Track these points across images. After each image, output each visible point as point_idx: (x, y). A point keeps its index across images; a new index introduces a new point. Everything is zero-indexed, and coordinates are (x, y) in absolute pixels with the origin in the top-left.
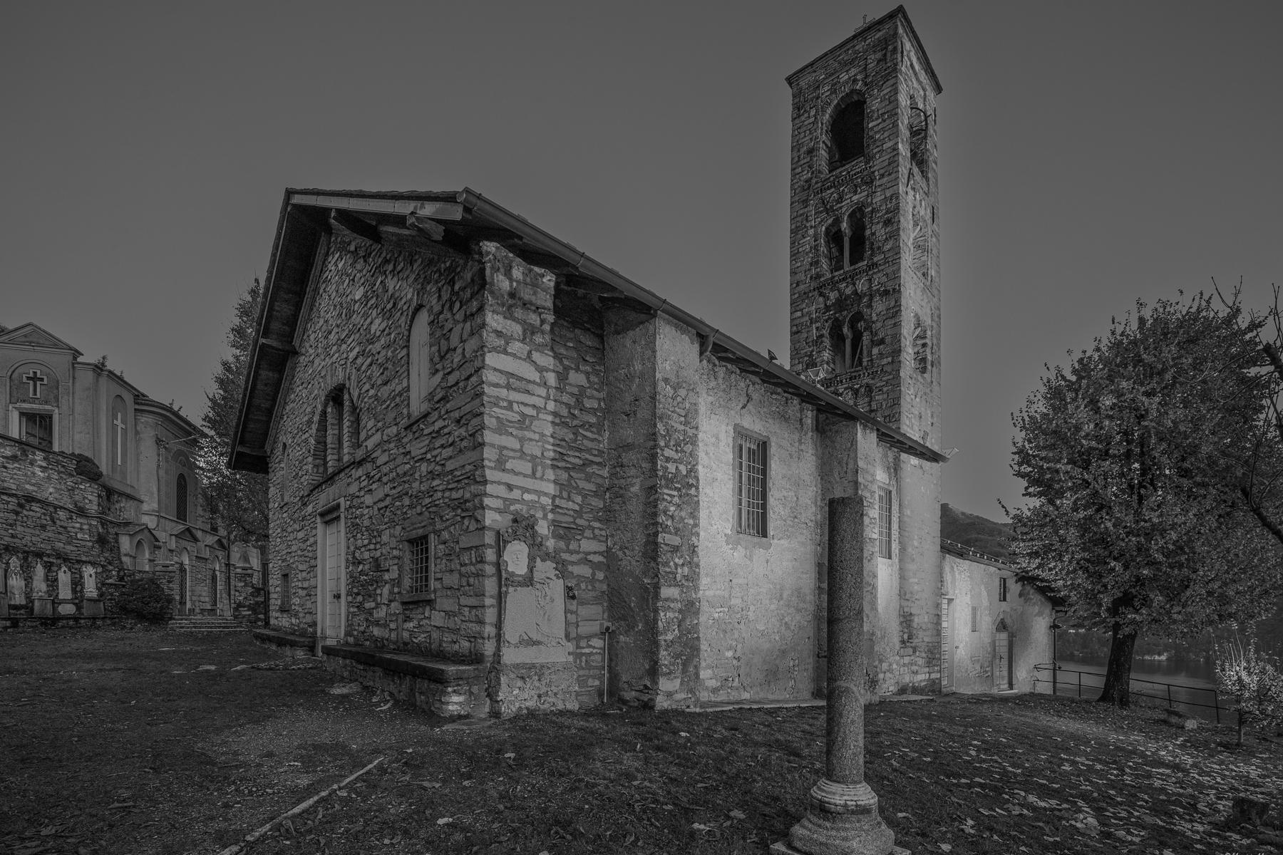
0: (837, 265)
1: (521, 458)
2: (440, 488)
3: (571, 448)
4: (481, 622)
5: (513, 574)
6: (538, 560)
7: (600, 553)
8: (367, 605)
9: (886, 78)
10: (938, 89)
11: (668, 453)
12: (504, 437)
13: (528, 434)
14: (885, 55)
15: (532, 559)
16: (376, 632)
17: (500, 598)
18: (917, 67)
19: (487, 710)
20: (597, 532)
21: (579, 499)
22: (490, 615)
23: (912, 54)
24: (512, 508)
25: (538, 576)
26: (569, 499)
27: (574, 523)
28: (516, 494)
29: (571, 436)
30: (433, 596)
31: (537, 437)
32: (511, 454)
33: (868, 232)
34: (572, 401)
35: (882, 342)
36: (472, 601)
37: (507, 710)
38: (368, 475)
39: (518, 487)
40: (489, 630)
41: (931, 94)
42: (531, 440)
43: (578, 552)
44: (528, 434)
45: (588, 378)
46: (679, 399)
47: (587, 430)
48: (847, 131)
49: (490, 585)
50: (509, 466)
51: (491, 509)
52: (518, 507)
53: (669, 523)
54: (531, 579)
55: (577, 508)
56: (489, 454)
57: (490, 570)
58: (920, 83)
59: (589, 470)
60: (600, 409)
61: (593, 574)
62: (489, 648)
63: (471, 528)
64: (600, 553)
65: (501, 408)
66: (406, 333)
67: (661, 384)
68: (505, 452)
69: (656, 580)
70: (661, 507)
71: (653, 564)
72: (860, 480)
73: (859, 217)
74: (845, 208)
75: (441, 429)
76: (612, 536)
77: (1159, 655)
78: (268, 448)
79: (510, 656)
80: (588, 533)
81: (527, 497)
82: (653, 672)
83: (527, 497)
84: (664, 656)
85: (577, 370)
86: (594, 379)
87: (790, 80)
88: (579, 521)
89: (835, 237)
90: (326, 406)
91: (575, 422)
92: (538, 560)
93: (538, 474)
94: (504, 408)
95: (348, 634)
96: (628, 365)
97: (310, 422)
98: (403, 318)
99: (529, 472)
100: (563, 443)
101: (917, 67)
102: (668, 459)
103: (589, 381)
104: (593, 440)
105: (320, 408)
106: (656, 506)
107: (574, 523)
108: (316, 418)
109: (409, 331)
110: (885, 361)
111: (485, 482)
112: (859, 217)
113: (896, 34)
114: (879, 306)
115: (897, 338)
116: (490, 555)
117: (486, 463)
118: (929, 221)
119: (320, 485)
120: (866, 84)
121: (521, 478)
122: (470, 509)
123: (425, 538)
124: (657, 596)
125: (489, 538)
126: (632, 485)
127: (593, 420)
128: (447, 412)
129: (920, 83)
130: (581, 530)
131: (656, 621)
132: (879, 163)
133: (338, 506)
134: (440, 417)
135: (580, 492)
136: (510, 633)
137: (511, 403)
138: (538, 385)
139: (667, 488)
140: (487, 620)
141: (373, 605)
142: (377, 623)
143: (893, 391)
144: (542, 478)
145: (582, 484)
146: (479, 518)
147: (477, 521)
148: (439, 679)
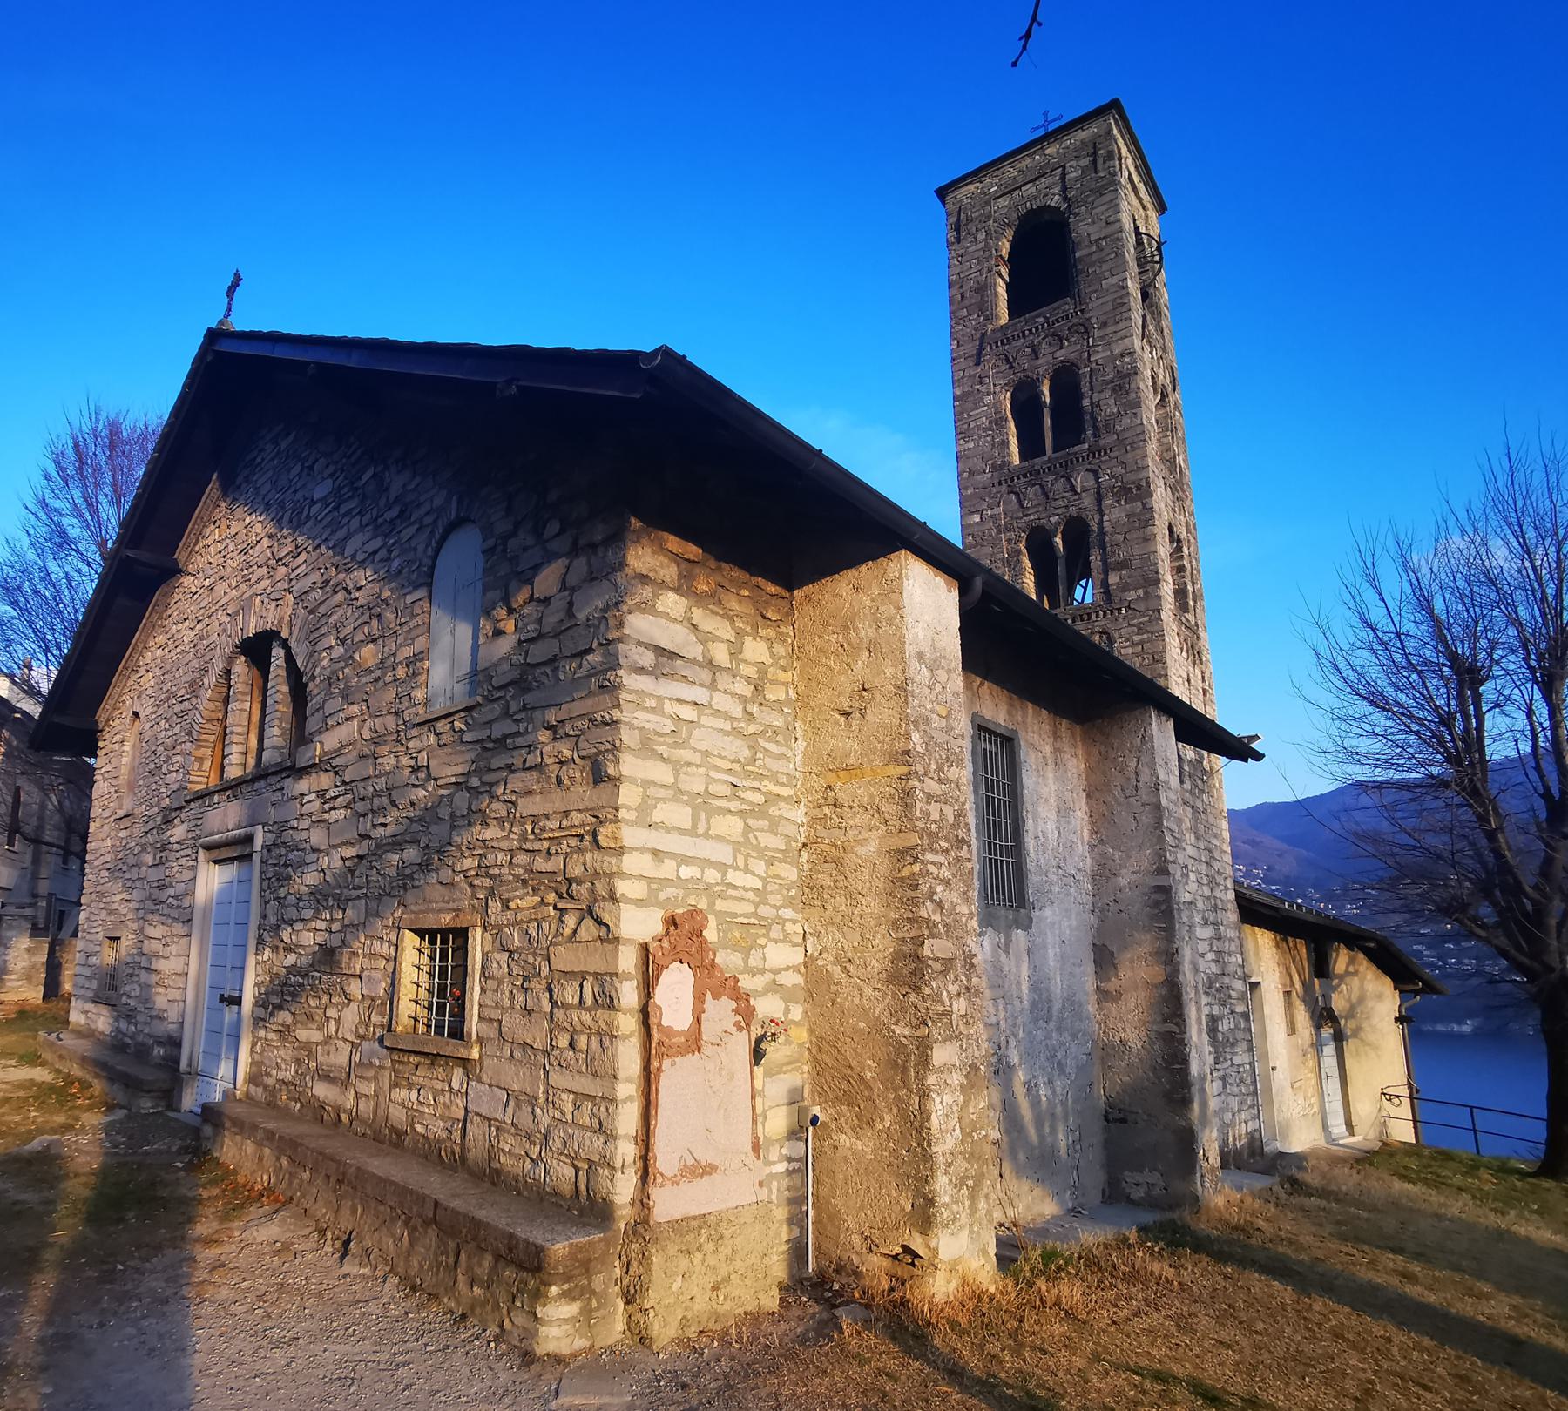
0: (1031, 446)
1: (675, 799)
2: (505, 845)
3: (748, 775)
4: (604, 1130)
5: (669, 1032)
6: (709, 995)
7: (796, 969)
8: (303, 1034)
9: (1099, 192)
10: (1162, 208)
11: (932, 786)
12: (650, 763)
13: (684, 754)
14: (1094, 162)
15: (699, 997)
16: (322, 1090)
17: (648, 1078)
18: (1136, 179)
19: (620, 1326)
20: (789, 927)
21: (760, 867)
22: (627, 1119)
23: (1129, 161)
24: (662, 896)
25: (709, 1030)
26: (747, 870)
27: (756, 915)
28: (668, 869)
29: (747, 753)
30: (475, 1054)
31: (697, 758)
32: (662, 793)
33: (1086, 402)
34: (747, 690)
35: (1124, 565)
36: (585, 1084)
37: (664, 1331)
38: (321, 794)
39: (673, 856)
40: (626, 1150)
41: (1153, 214)
42: (689, 764)
43: (762, 971)
44: (684, 754)
45: (770, 648)
46: (938, 688)
47: (769, 740)
48: (1047, 262)
49: (629, 1058)
50: (657, 816)
51: (629, 901)
52: (671, 892)
53: (937, 918)
54: (698, 1039)
55: (759, 885)
56: (628, 795)
57: (628, 1023)
58: (1140, 200)
59: (773, 811)
60: (788, 701)
61: (787, 1011)
62: (623, 1190)
63: (583, 934)
64: (796, 969)
65: (646, 710)
66: (427, 561)
67: (915, 664)
68: (652, 791)
69: (924, 1031)
70: (925, 888)
71: (913, 997)
72: (1164, 802)
73: (1067, 380)
74: (1044, 365)
75: (506, 737)
76: (818, 935)
77: (1460, 1023)
78: (101, 716)
79: (667, 1204)
80: (776, 932)
81: (686, 872)
82: (924, 1215)
83: (686, 872)
84: (942, 1185)
85: (756, 635)
86: (780, 650)
87: (942, 193)
88: (764, 911)
89: (1026, 408)
90: (230, 660)
91: (752, 729)
92: (709, 995)
93: (701, 830)
94: (653, 710)
95: (253, 1079)
96: (845, 629)
97: (194, 687)
98: (423, 536)
99: (687, 825)
100: (736, 766)
101: (1136, 179)
102: (930, 797)
103: (772, 655)
104: (778, 757)
105: (220, 665)
106: (915, 887)
107: (756, 915)
108: (211, 679)
109: (435, 559)
110: (1132, 595)
111: (620, 851)
112: (1067, 380)
113: (1109, 132)
114: (1115, 513)
115: (1149, 560)
116: (629, 994)
117: (623, 814)
118: (1170, 389)
119: (211, 794)
120: (1066, 199)
121: (675, 837)
122: (591, 904)
123: (462, 934)
124: (924, 1061)
125: (628, 960)
126: (861, 843)
127: (779, 722)
128: (524, 708)
129: (1140, 200)
130: (765, 925)
131: (924, 1114)
132: (1096, 308)
133: (249, 839)
134: (506, 714)
135: (762, 851)
136: (666, 1159)
137: (660, 699)
138: (701, 666)
139: (932, 850)
140: (621, 1132)
141: (317, 1036)
142: (325, 1076)
143: (1150, 640)
144: (706, 835)
145: (767, 840)
146: (606, 918)
147: (599, 922)
148: (530, 1264)
